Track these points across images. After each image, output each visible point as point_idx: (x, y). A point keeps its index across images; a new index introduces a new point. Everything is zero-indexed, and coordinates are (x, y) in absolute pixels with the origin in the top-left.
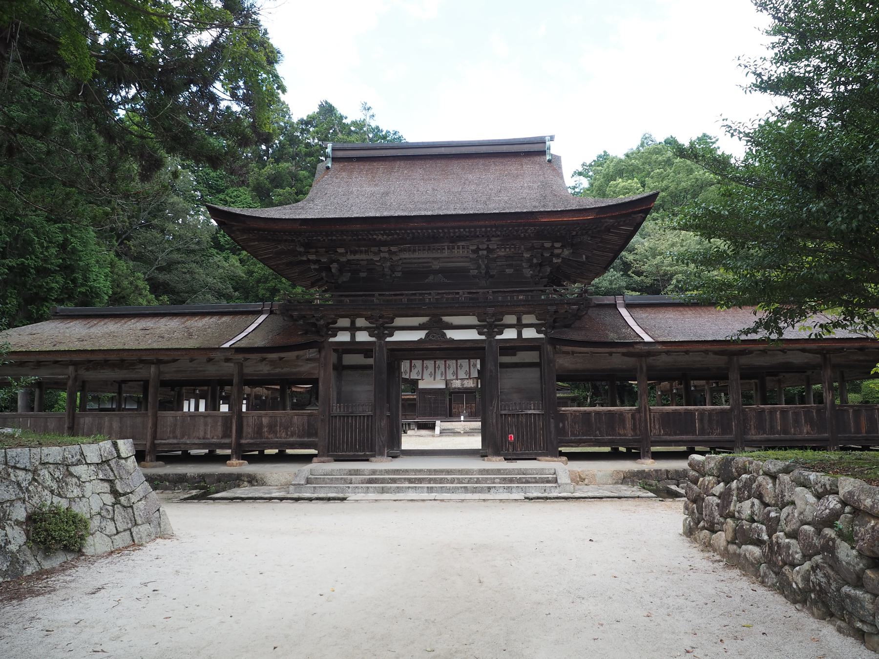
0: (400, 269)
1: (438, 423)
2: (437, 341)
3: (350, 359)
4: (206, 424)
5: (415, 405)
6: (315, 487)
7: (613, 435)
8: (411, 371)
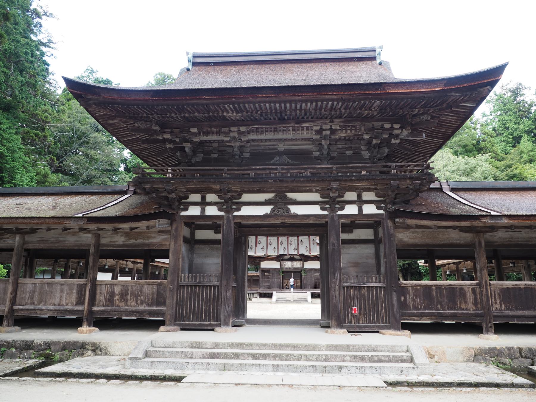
0: (248, 150)
1: (274, 293)
2: (282, 216)
3: (201, 234)
4: (62, 291)
5: (258, 280)
6: (152, 362)
7: (455, 309)
8: (256, 246)
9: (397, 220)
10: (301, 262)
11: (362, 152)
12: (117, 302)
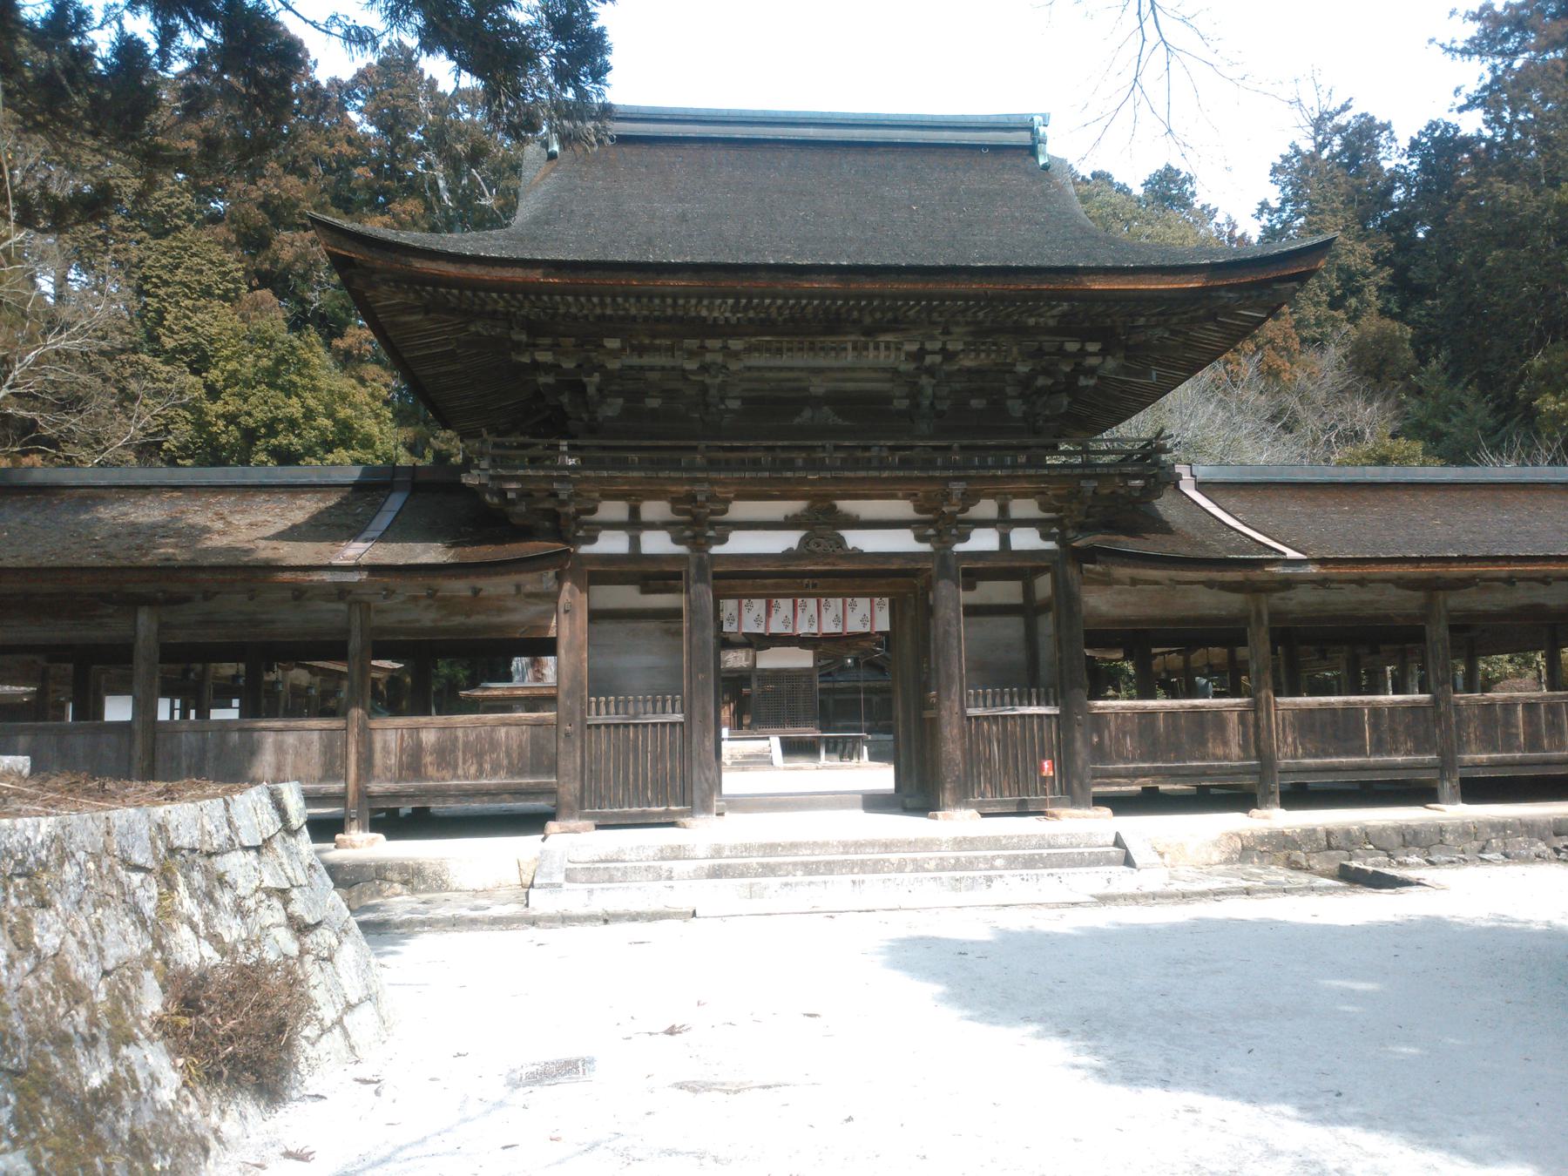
2: (827, 555)
7: (1203, 759)
9: (1086, 566)
10: (751, 652)
11: (1009, 403)
12: (431, 770)
